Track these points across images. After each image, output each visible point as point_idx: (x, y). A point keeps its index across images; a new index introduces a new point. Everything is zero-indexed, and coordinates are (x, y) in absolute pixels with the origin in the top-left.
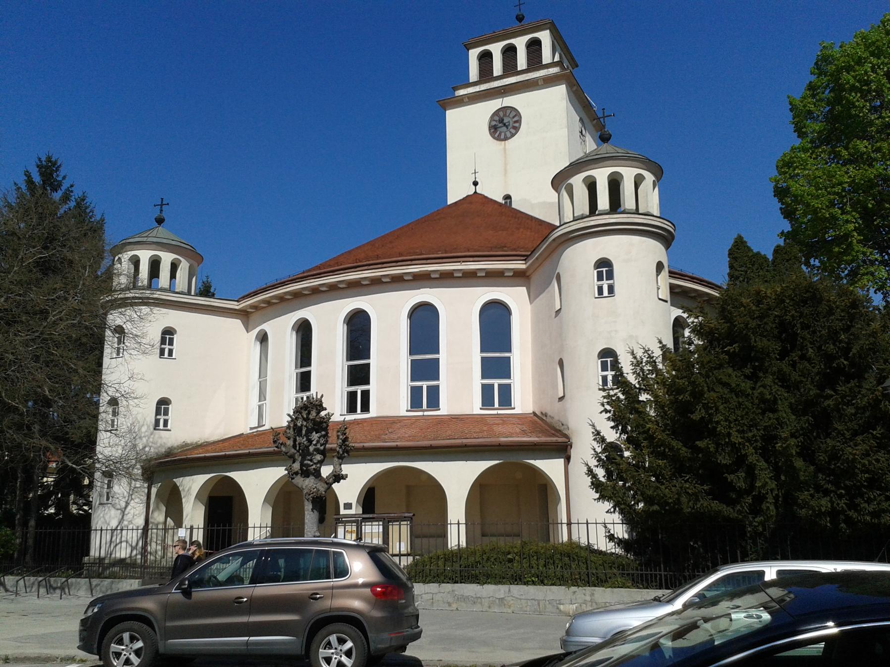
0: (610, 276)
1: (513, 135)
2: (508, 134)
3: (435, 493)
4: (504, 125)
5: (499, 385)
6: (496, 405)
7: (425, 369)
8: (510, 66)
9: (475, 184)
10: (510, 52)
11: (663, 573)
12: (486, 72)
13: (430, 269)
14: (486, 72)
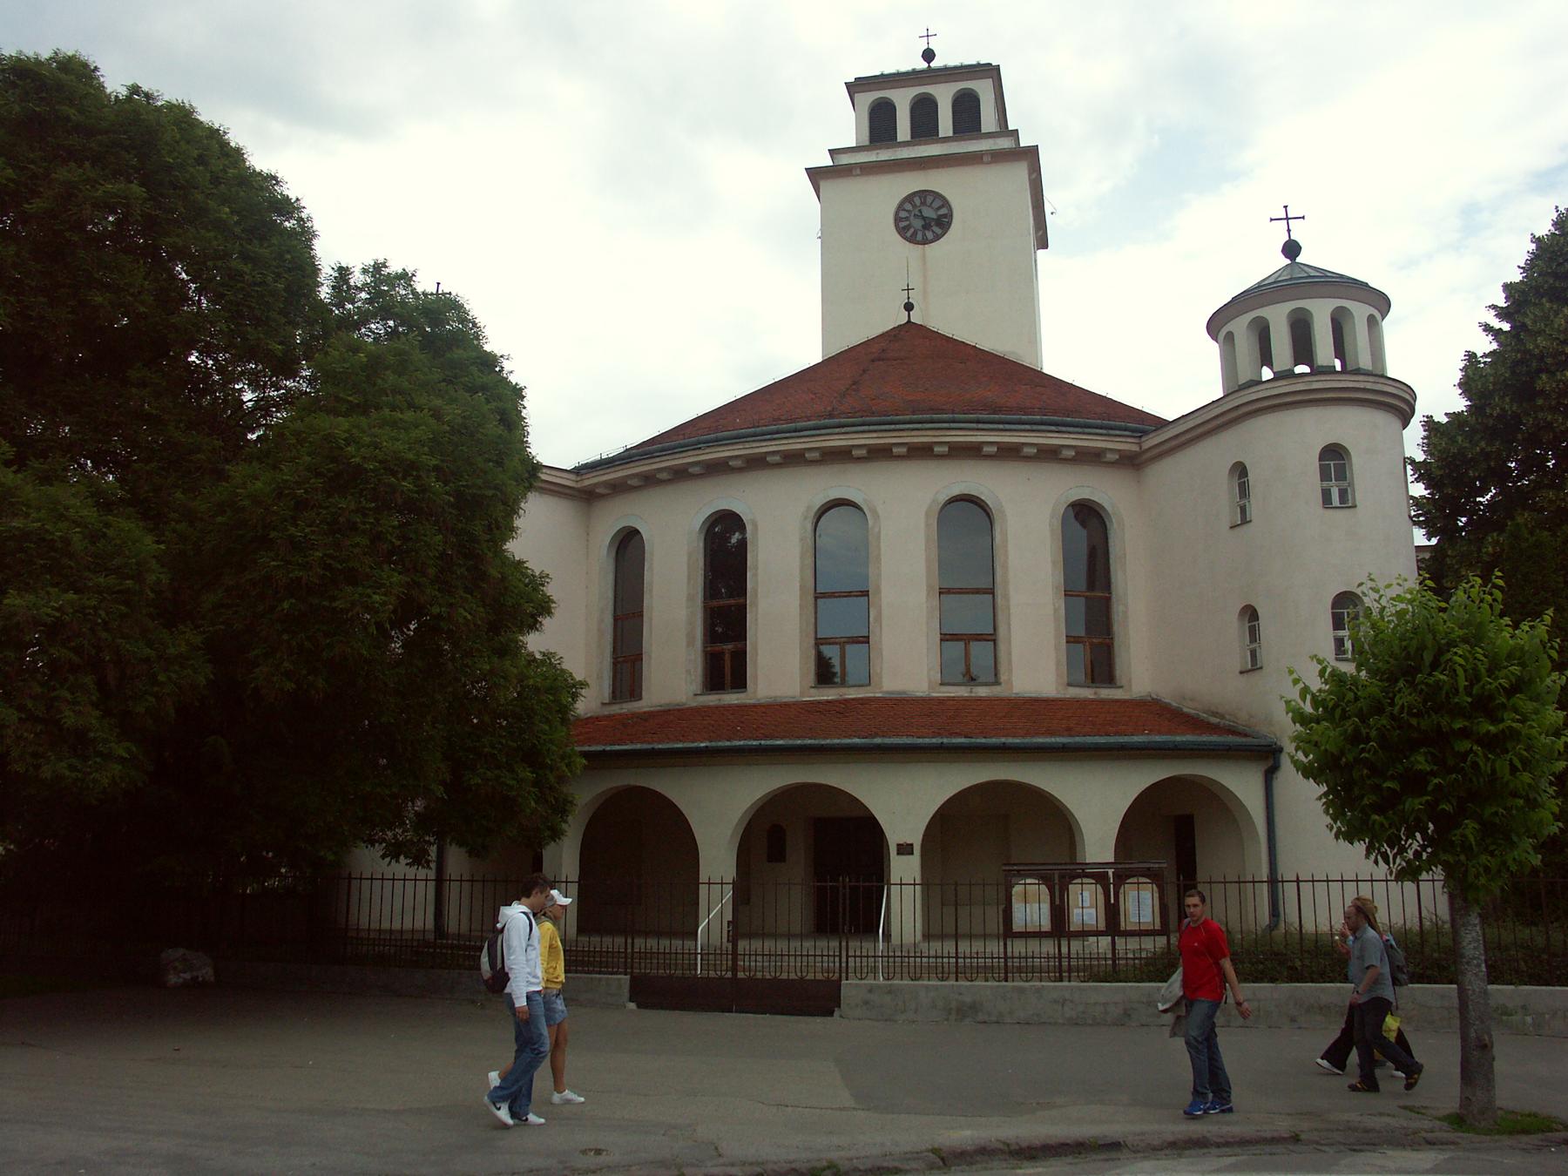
0: (1342, 474)
1: (937, 238)
3: (1058, 822)
6: (727, 657)
9: (909, 307)
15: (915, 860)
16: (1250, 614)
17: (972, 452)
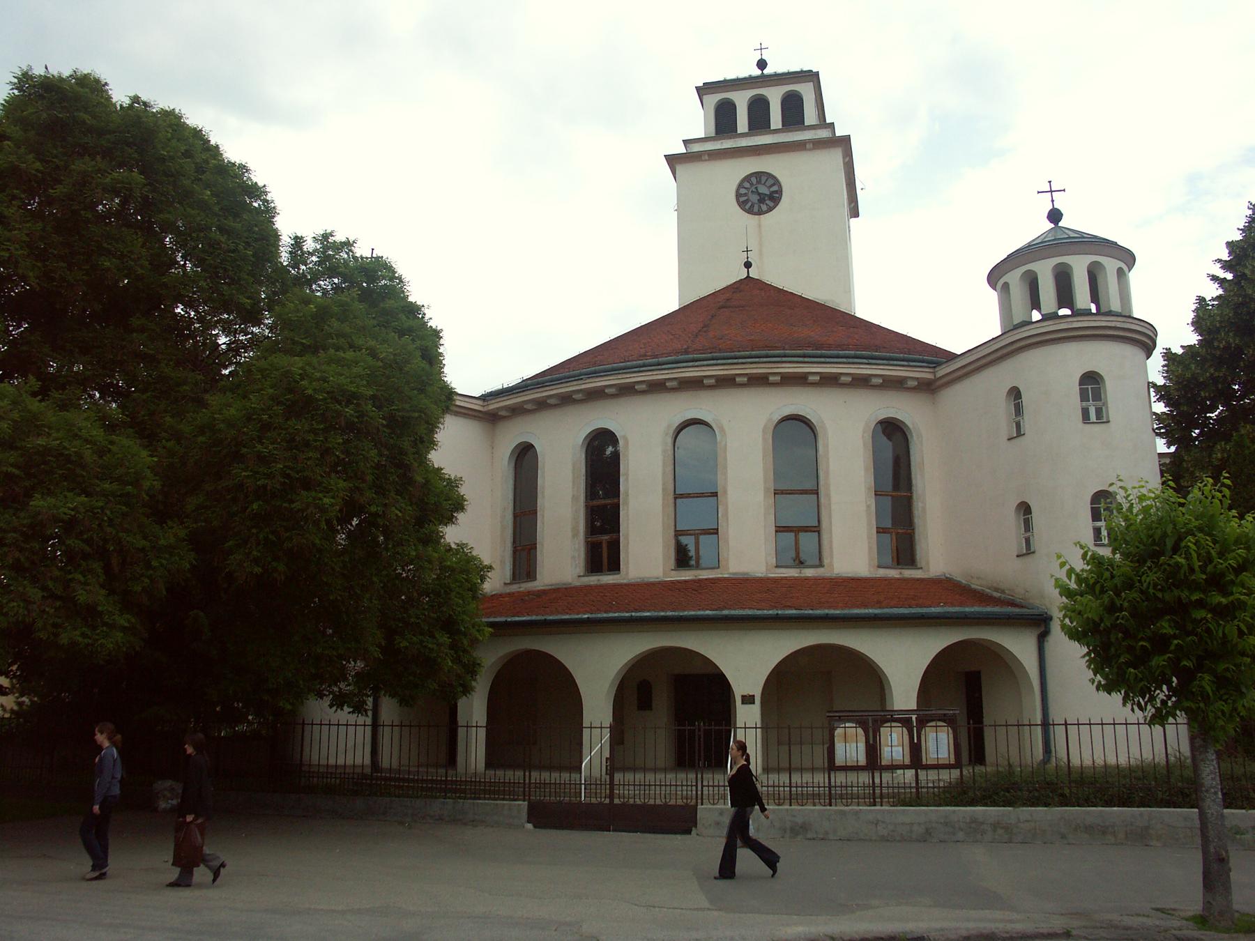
0: (1098, 396)
1: (770, 209)
3: (870, 676)
9: (748, 265)
13: (869, 372)
17: (800, 380)
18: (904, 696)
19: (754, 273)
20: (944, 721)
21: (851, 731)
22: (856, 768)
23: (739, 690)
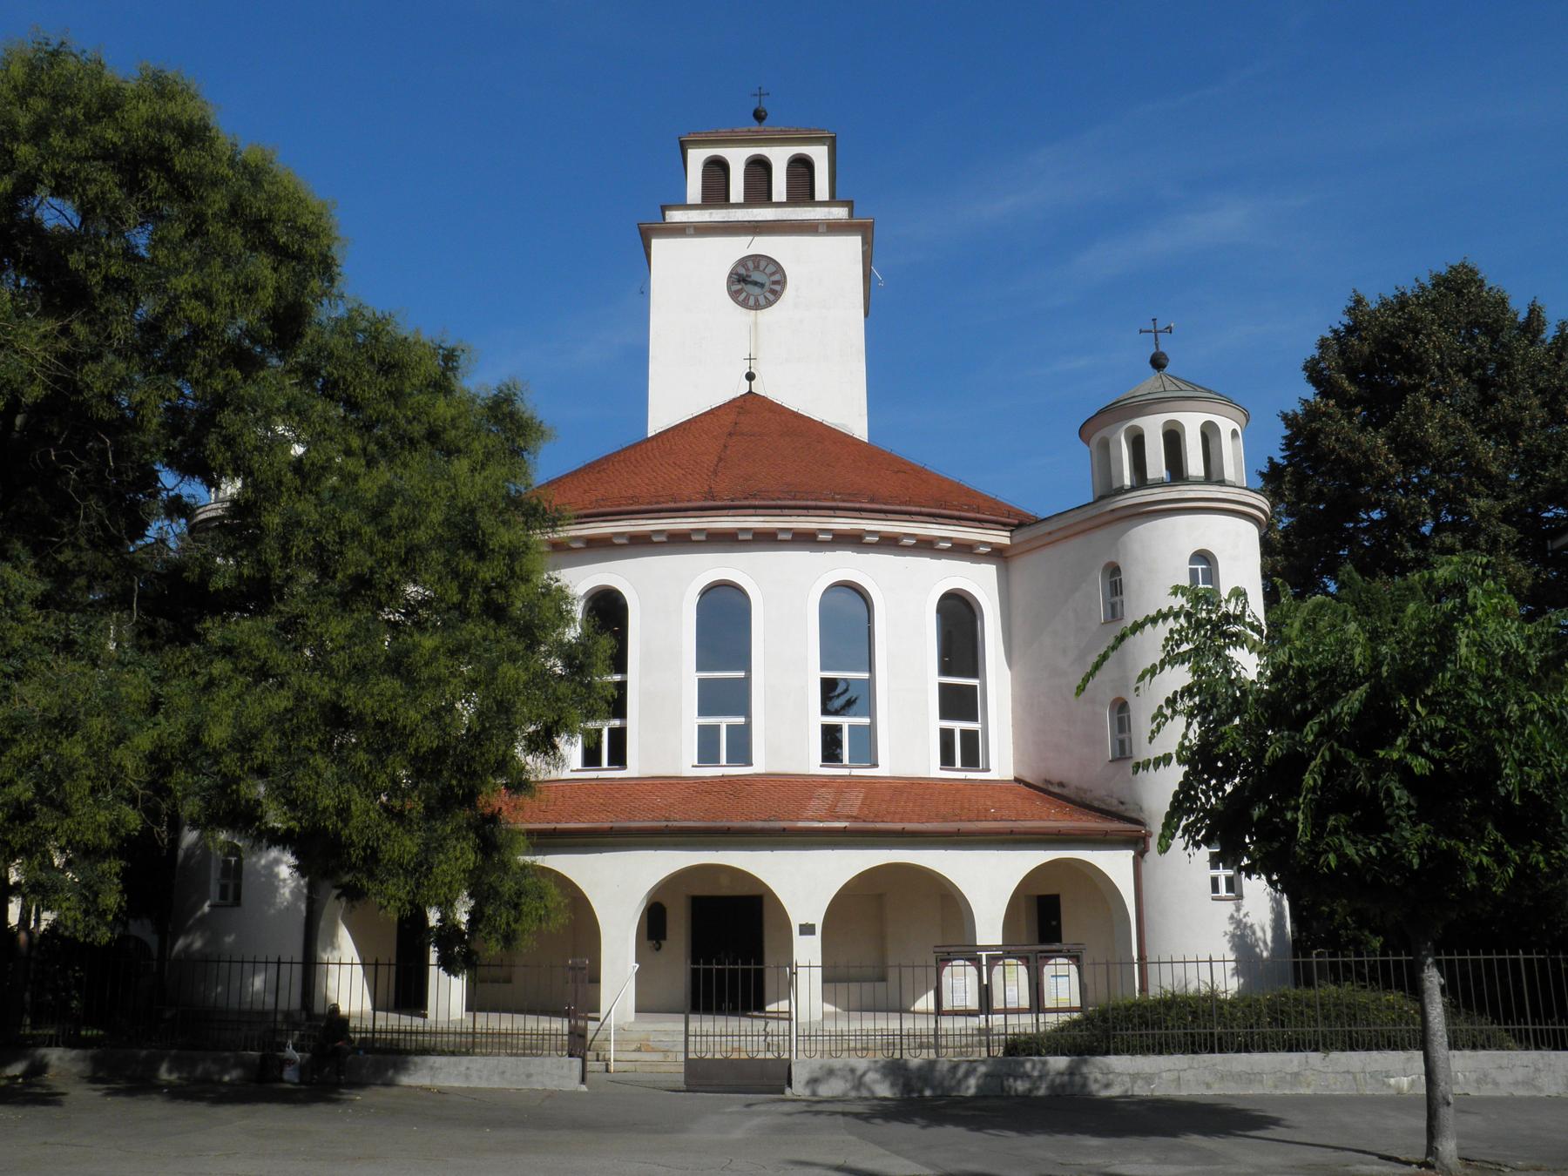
1: (770, 304)
2: (762, 301)
3: (948, 902)
4: (755, 284)
5: (963, 732)
6: (723, 760)
7: (725, 696)
8: (758, 189)
9: (750, 377)
10: (759, 169)
11: (1530, 1027)
12: (716, 189)
14: (716, 189)
15: (815, 941)
16: (1081, 689)
17: (853, 541)
18: (989, 930)
19: (758, 388)
20: (1019, 958)
21: (1062, 970)
22: (968, 1013)
23: (796, 919)
